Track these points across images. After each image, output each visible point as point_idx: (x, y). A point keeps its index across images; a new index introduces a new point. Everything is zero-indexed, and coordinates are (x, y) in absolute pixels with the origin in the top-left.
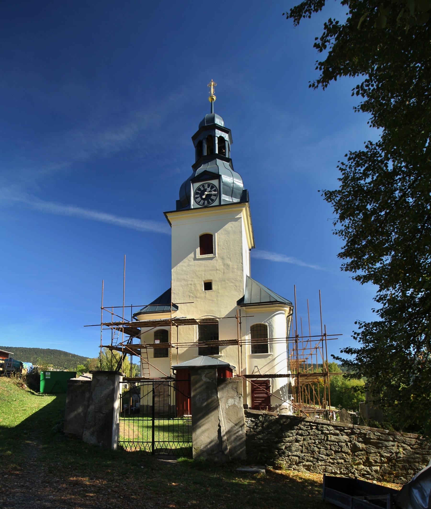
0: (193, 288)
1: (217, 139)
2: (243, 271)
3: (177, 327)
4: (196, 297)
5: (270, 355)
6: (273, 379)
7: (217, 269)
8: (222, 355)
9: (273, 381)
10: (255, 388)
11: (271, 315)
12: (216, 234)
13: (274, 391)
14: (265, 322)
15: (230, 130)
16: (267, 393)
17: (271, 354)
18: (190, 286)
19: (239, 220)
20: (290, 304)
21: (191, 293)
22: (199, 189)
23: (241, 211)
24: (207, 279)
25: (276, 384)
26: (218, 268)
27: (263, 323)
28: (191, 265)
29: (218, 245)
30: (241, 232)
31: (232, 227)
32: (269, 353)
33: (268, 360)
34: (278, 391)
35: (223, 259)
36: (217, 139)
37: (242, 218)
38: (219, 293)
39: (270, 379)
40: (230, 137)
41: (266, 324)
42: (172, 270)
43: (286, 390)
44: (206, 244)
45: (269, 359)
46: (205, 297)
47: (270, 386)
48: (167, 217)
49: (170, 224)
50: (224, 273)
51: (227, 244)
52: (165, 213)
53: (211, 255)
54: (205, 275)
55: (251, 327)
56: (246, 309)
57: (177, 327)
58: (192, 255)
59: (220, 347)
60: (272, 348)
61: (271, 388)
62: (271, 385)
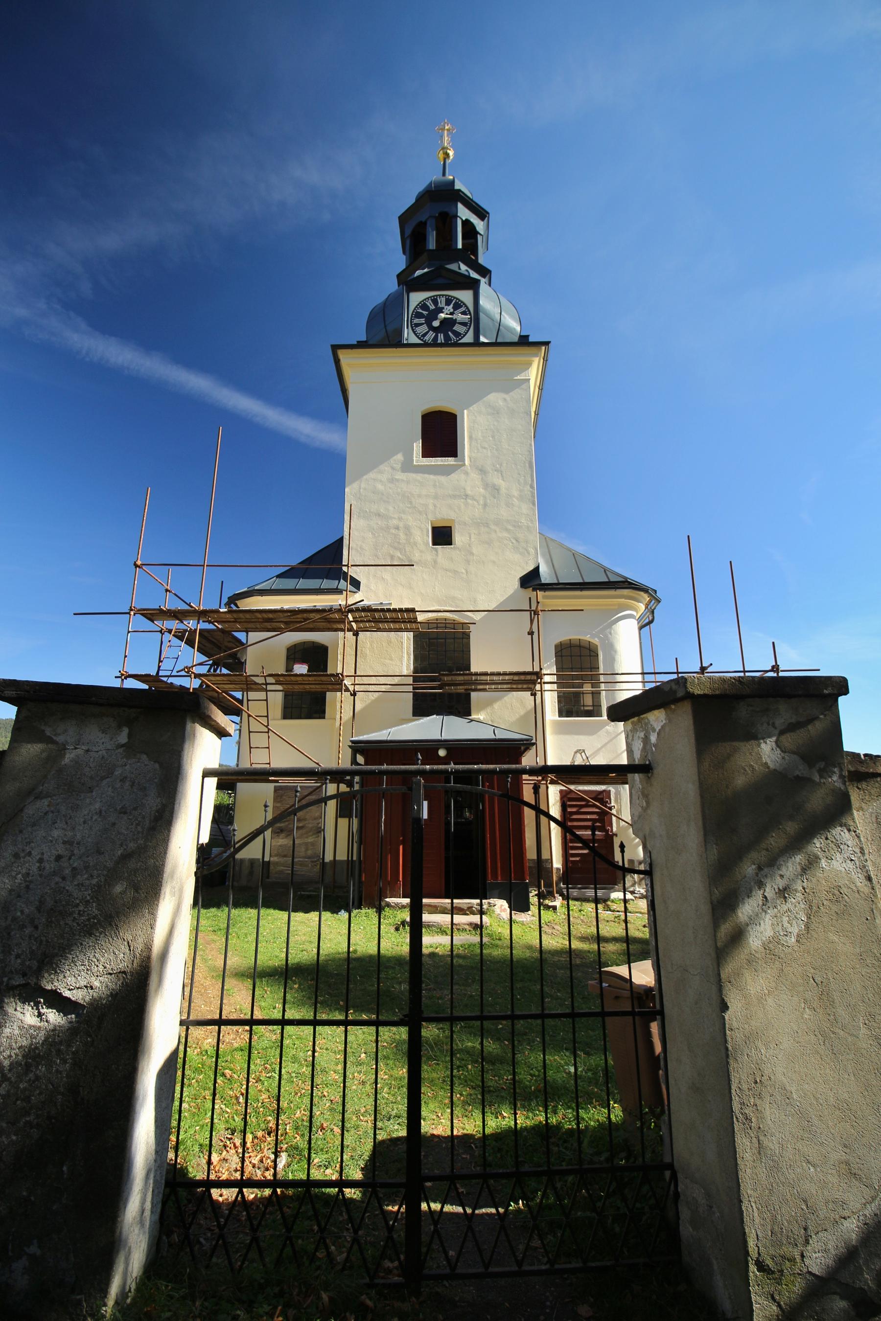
0: (402, 536)
3: (356, 634)
7: (467, 496)
11: (610, 618)
14: (593, 636)
15: (488, 213)
18: (393, 531)
19: (524, 386)
21: (396, 548)
22: (423, 305)
23: (530, 364)
24: (439, 516)
26: (469, 492)
27: (588, 638)
28: (398, 480)
29: (470, 438)
31: (505, 400)
35: (482, 471)
38: (472, 554)
39: (612, 789)
41: (596, 641)
42: (346, 490)
44: (440, 434)
45: (608, 732)
46: (435, 562)
50: (485, 505)
51: (493, 437)
52: (335, 348)
53: (450, 461)
54: (435, 506)
55: (556, 646)
57: (356, 634)
58: (400, 457)
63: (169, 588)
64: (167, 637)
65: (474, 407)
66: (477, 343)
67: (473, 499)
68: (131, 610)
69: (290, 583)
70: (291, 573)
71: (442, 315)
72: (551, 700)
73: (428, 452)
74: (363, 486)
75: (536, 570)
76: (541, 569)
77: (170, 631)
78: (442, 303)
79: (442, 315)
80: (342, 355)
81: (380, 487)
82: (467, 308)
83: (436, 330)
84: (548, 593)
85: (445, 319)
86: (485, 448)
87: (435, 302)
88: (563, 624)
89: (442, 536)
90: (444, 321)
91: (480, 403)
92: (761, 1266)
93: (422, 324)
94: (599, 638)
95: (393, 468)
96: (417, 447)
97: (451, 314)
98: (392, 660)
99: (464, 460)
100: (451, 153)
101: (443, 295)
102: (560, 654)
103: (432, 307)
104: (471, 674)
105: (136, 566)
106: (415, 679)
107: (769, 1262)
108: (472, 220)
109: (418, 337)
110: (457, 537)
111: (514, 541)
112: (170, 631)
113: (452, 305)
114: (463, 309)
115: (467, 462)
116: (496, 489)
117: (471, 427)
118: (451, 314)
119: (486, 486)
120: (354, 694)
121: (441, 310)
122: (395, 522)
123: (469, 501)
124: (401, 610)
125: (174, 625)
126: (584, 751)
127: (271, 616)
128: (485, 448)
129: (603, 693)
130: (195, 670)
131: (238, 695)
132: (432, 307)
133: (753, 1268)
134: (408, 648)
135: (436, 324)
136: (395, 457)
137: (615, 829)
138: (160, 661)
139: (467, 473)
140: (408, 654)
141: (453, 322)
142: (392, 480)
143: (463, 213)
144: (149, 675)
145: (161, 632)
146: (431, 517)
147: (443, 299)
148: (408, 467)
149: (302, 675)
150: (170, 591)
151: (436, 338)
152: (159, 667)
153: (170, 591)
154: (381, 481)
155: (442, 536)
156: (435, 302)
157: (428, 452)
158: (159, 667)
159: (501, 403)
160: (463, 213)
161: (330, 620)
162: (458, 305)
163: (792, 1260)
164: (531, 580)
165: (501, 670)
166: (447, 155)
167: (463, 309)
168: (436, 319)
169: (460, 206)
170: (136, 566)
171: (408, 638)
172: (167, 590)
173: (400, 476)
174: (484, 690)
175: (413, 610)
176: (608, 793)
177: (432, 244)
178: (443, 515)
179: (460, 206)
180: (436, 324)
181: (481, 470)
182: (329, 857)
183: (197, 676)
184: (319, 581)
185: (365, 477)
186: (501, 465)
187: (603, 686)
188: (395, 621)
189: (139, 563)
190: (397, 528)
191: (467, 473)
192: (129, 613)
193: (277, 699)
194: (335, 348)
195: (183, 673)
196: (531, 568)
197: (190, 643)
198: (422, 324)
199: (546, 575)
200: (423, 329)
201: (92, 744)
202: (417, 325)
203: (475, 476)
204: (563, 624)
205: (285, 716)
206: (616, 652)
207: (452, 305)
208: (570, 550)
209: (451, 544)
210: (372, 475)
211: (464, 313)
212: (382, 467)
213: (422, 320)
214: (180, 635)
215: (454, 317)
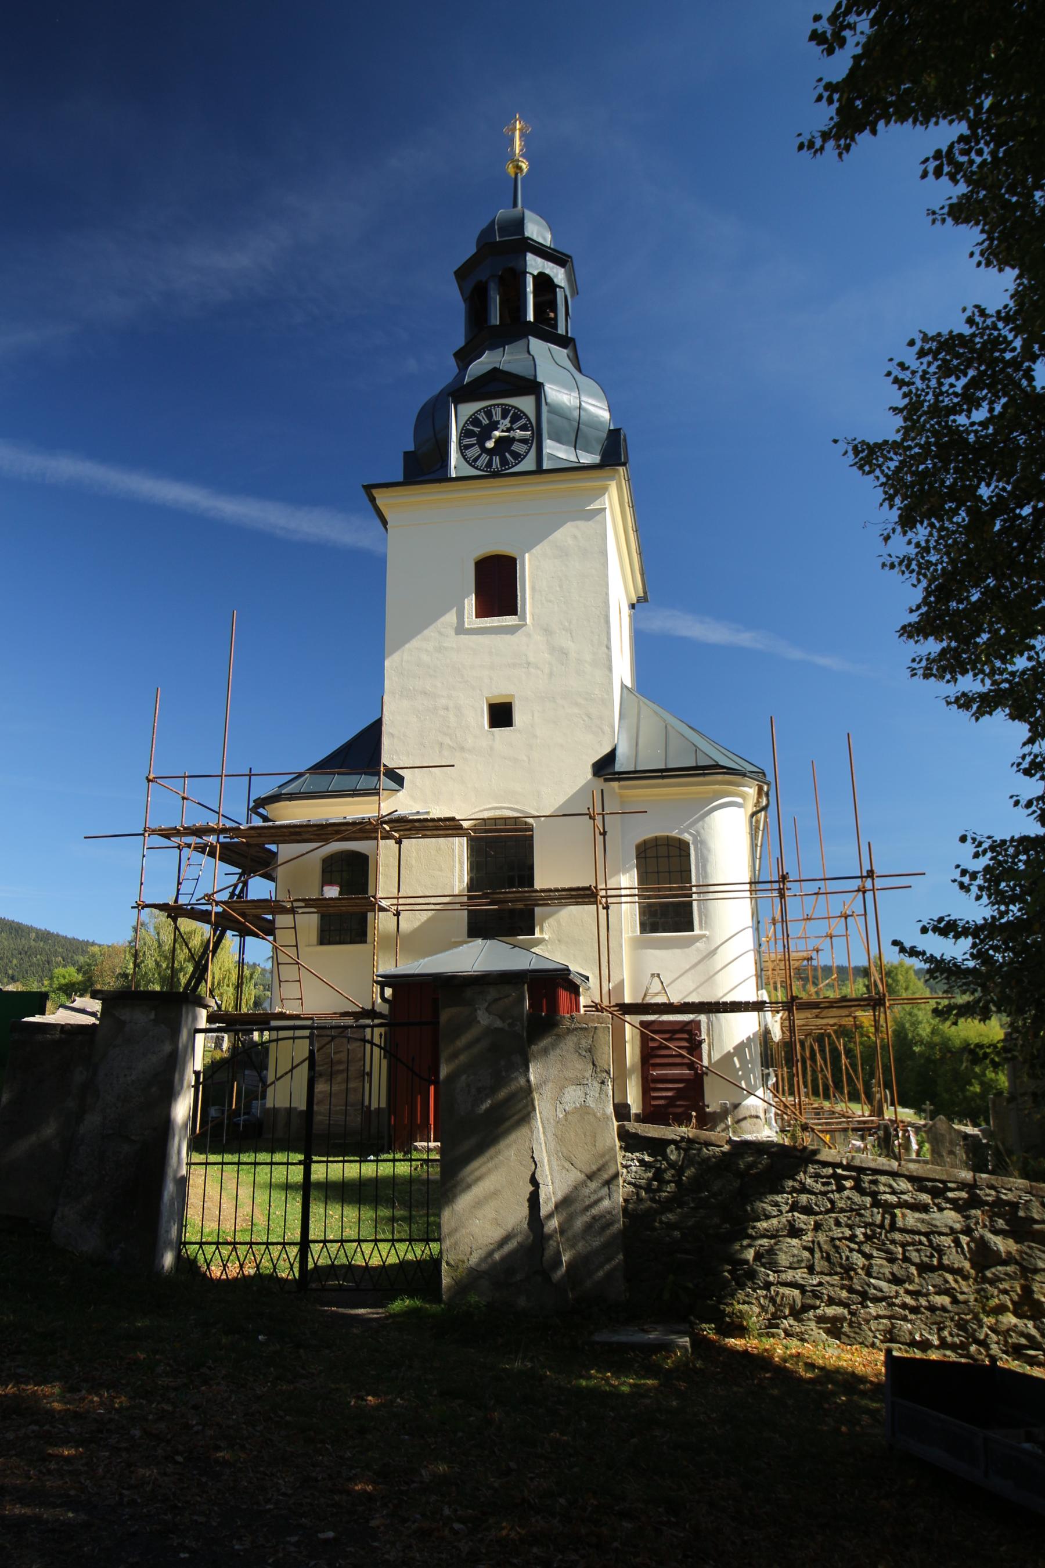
1: (530, 280)
2: (610, 669)
3: (399, 842)
4: (462, 749)
5: (700, 937)
6: (713, 1016)
7: (529, 664)
8: (546, 937)
9: (710, 1024)
10: (653, 1048)
11: (702, 808)
12: (527, 555)
13: (716, 1056)
14: (682, 832)
15: (569, 257)
16: (691, 1066)
17: (704, 936)
18: (442, 712)
19: (598, 518)
20: (760, 775)
22: (474, 420)
23: (605, 490)
25: (720, 1035)
26: (531, 659)
27: (675, 833)
29: (533, 589)
30: (604, 553)
31: (575, 537)
32: (697, 931)
33: (693, 954)
34: (728, 1056)
35: (547, 631)
36: (530, 280)
37: (608, 511)
38: (535, 736)
40: (571, 277)
41: (686, 837)
42: (386, 663)
43: (754, 1053)
44: (497, 587)
45: (698, 950)
46: (492, 748)
47: (701, 1042)
48: (373, 500)
49: (385, 523)
50: (551, 675)
51: (561, 586)
52: (368, 488)
55: (638, 847)
56: (621, 787)
57: (399, 842)
58: (451, 617)
59: (537, 909)
60: (704, 914)
61: (705, 1047)
62: (704, 1036)
63: (186, 796)
64: (186, 852)
65: (537, 550)
66: (539, 471)
67: (537, 667)
68: (145, 831)
69: (323, 782)
70: (325, 766)
71: (497, 433)
72: (627, 915)
73: (484, 610)
74: (406, 657)
75: (613, 753)
76: (619, 752)
77: (189, 846)
78: (497, 414)
79: (497, 433)
80: (376, 493)
81: (425, 658)
82: (529, 419)
83: (490, 452)
84: (622, 783)
85: (500, 438)
86: (550, 601)
87: (488, 413)
88: (655, 814)
89: (501, 715)
90: (499, 441)
91: (545, 542)
92: (448, 1264)
93: (474, 445)
94: (690, 834)
95: (440, 633)
96: (470, 603)
97: (508, 430)
98: (441, 870)
99: (523, 618)
100: (524, 166)
101: (498, 405)
102: (643, 855)
103: (485, 422)
104: (537, 891)
105: (149, 781)
106: (470, 897)
107: (452, 1262)
108: (547, 272)
109: (468, 462)
110: (517, 717)
111: (586, 719)
112: (189, 846)
113: (509, 419)
114: (523, 421)
115: (529, 621)
116: (564, 652)
117: (534, 574)
118: (508, 430)
119: (552, 649)
120: (397, 914)
121: (494, 426)
122: (444, 701)
123: (532, 670)
124: (440, 820)
125: (192, 840)
126: (658, 976)
127: (297, 830)
128: (550, 601)
129: (695, 904)
130: (217, 897)
131: (270, 917)
132: (485, 422)
133: (444, 1264)
134: (461, 856)
135: (490, 444)
136: (442, 619)
137: (705, 1063)
138: (179, 883)
139: (528, 635)
140: (461, 863)
141: (511, 441)
142: (440, 649)
143: (535, 264)
144: (167, 905)
145: (178, 847)
146: (487, 693)
147: (499, 410)
148: (460, 630)
149: (331, 899)
150: (187, 799)
151: (489, 464)
152: (178, 890)
153: (187, 799)
154: (426, 650)
155: (501, 715)
156: (488, 413)
157: (484, 610)
158: (178, 890)
159: (570, 541)
160: (535, 264)
161: (365, 830)
162: (517, 416)
163: (463, 1262)
164: (605, 767)
165: (559, 886)
166: (520, 168)
167: (523, 421)
168: (490, 438)
169: (530, 257)
170: (149, 781)
171: (461, 844)
172: (184, 798)
173: (453, 640)
174: (547, 905)
175: (453, 819)
176: (698, 1024)
177: (495, 320)
178: (499, 692)
179: (530, 257)
180: (490, 444)
181: (546, 630)
182: (374, 1106)
183: (217, 903)
184: (355, 777)
185: (407, 646)
186: (570, 623)
187: (695, 896)
188: (437, 828)
189: (151, 777)
190: (447, 709)
191: (528, 635)
192: (143, 834)
193: (309, 922)
194: (368, 488)
195: (203, 901)
196: (607, 750)
197: (212, 854)
198: (474, 445)
199: (621, 764)
200: (475, 451)
201: (139, 1018)
202: (468, 447)
203: (539, 638)
204: (655, 814)
205: (322, 942)
206: (709, 850)
207: (509, 419)
208: (665, 721)
209: (511, 725)
210: (415, 643)
211: (523, 428)
212: (426, 632)
213: (473, 440)
214: (201, 849)
215: (512, 434)
